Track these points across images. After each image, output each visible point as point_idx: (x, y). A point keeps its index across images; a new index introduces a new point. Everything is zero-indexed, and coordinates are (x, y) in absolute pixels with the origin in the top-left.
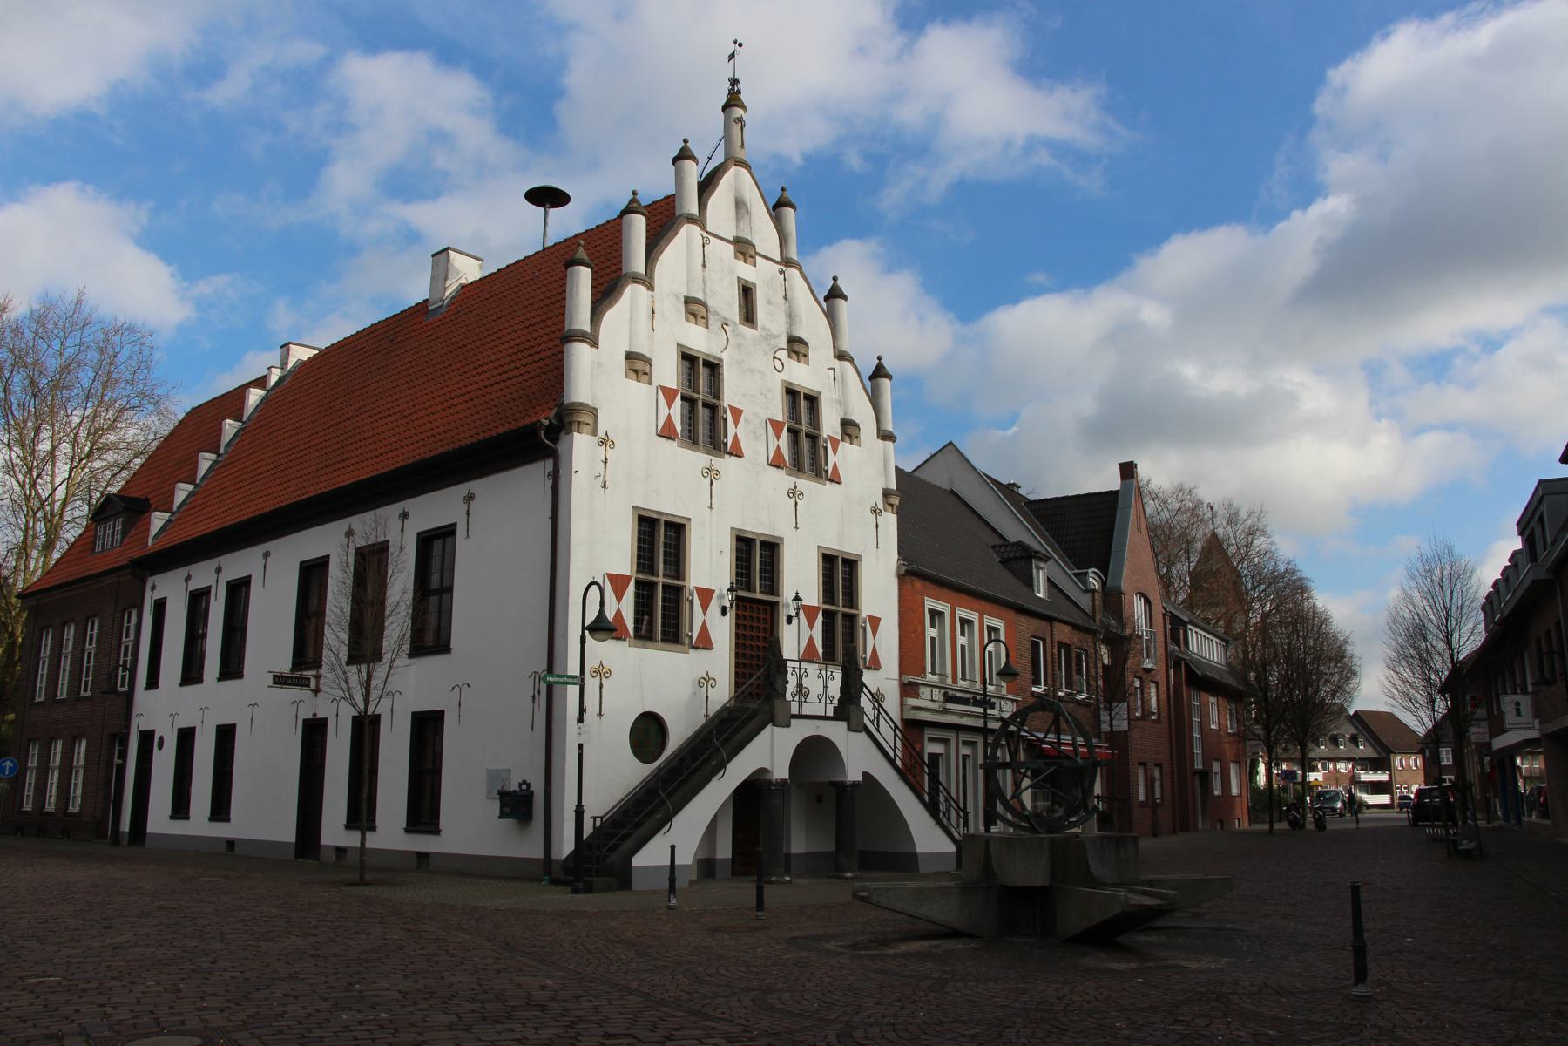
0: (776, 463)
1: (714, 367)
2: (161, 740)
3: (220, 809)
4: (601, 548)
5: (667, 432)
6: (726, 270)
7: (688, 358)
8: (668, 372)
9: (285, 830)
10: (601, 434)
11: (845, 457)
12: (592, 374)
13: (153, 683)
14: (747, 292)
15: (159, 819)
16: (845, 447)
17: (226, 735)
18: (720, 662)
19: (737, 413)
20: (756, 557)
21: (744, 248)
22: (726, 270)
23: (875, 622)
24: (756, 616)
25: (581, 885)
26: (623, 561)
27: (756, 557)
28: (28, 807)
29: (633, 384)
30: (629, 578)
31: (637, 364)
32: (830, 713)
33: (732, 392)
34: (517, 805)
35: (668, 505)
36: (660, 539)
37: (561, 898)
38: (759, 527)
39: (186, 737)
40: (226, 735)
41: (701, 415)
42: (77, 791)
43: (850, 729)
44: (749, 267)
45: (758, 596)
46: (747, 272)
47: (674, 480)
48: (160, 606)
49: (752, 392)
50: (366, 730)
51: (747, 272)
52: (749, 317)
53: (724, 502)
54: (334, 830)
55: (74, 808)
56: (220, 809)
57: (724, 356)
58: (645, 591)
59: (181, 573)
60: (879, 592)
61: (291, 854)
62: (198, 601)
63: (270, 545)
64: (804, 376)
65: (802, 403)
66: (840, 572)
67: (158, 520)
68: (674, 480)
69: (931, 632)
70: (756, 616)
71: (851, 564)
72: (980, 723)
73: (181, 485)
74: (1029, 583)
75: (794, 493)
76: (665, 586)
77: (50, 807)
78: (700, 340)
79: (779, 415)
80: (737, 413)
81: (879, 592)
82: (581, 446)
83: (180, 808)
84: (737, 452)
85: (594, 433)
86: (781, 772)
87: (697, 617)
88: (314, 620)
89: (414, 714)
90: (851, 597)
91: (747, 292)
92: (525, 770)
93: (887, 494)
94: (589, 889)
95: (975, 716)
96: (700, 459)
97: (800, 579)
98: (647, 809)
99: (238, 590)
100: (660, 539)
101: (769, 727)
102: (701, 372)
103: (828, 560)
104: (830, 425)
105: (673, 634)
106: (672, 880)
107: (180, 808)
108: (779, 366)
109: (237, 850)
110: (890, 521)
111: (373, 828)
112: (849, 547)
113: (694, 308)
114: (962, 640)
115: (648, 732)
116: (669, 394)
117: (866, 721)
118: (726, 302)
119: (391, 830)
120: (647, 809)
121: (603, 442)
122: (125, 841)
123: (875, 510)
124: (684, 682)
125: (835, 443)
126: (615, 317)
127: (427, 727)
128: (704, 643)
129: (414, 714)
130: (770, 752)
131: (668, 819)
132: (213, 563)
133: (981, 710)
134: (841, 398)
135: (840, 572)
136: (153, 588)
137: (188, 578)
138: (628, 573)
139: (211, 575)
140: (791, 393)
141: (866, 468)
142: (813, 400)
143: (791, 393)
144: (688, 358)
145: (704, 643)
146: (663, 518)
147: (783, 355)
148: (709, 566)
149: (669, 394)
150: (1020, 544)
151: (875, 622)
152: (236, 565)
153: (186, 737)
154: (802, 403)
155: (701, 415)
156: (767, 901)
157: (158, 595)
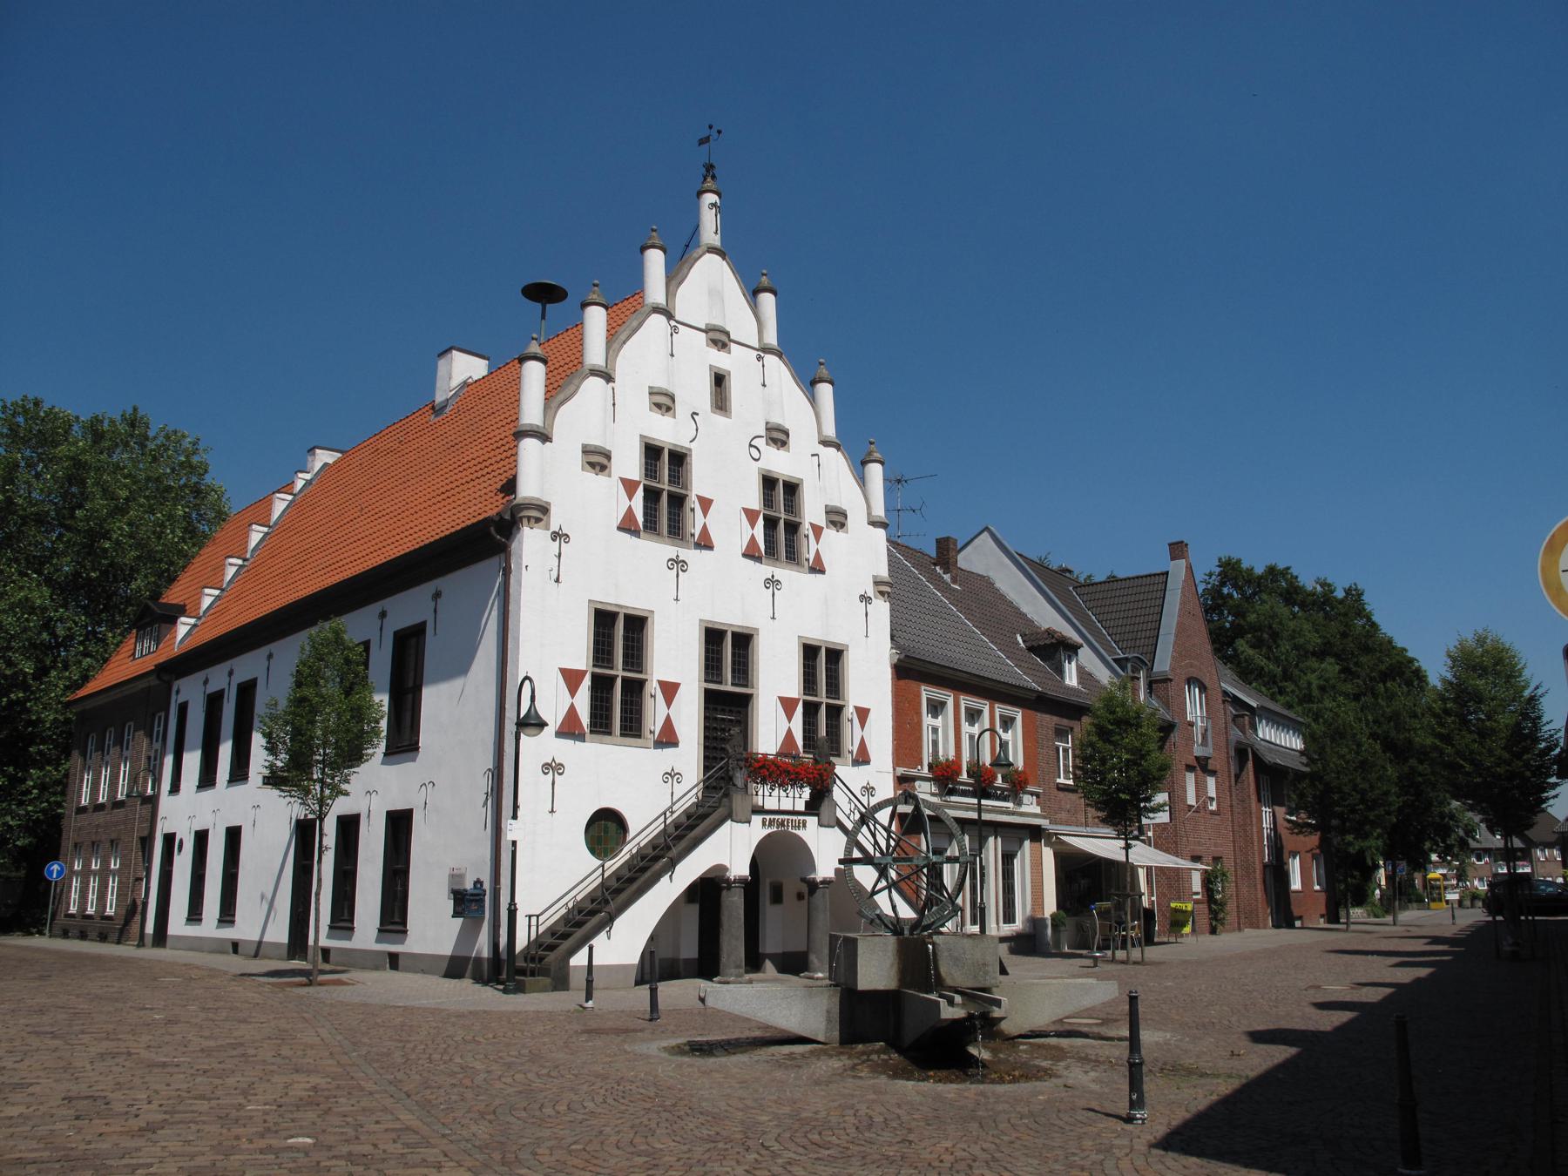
0: (751, 554)
1: (679, 459)
2: (181, 841)
3: (228, 913)
4: (550, 640)
5: (627, 526)
6: (699, 359)
7: (652, 452)
8: (629, 463)
9: (279, 933)
10: (554, 527)
11: (831, 545)
12: (541, 471)
13: (175, 789)
14: (719, 380)
15: (177, 923)
16: (830, 534)
17: (233, 835)
18: (689, 757)
19: (706, 504)
20: (728, 650)
21: (719, 339)
22: (699, 359)
23: (863, 714)
24: (727, 711)
25: (511, 985)
26: (580, 656)
27: (728, 650)
28: (73, 910)
29: (590, 476)
30: (584, 672)
31: (597, 460)
32: (801, 806)
33: (700, 481)
34: (466, 902)
35: (627, 599)
36: (619, 634)
37: (489, 997)
38: (731, 617)
39: (201, 838)
40: (233, 835)
41: (663, 498)
42: (111, 898)
43: (821, 825)
44: (722, 354)
45: (729, 688)
46: (721, 360)
47: (637, 574)
48: (183, 709)
49: (725, 486)
50: (349, 827)
51: (721, 360)
52: (721, 403)
53: (683, 599)
54: (320, 933)
55: (110, 912)
56: (228, 913)
57: (692, 446)
58: (601, 686)
59: (199, 677)
60: (869, 682)
61: (284, 952)
62: (214, 702)
63: (273, 647)
64: (781, 464)
65: (780, 494)
66: (822, 664)
67: (183, 626)
68: (637, 574)
69: (928, 720)
70: (727, 711)
71: (835, 656)
72: (974, 815)
73: (207, 591)
74: (1060, 671)
75: (772, 583)
76: (624, 680)
77: (90, 911)
78: (667, 432)
79: (755, 503)
80: (706, 504)
81: (869, 682)
82: (531, 543)
83: (195, 914)
84: (705, 543)
85: (547, 528)
86: (740, 868)
87: (655, 712)
88: (410, 696)
89: (389, 814)
90: (835, 686)
91: (719, 380)
92: (477, 870)
93: (877, 583)
94: (520, 989)
95: (967, 808)
96: (670, 550)
97: (776, 678)
98: (594, 912)
99: (247, 691)
100: (619, 634)
101: (729, 822)
102: (669, 465)
103: (810, 652)
104: (812, 512)
105: (633, 727)
106: (589, 982)
107: (195, 914)
108: (756, 455)
109: (332, 956)
110: (881, 610)
111: (1239, 561)
112: (835, 637)
113: (663, 402)
114: (966, 728)
115: (605, 828)
116: (629, 486)
117: (839, 814)
118: (695, 392)
119: (209, 926)
120: (594, 912)
121: (556, 536)
122: (149, 940)
123: (865, 598)
124: (649, 782)
125: (817, 531)
126: (566, 415)
127: (399, 825)
128: (668, 738)
129: (389, 814)
130: (731, 849)
131: (610, 920)
132: (224, 667)
133: (975, 801)
134: (827, 480)
135: (822, 664)
136: (178, 692)
137: (206, 682)
138: (584, 668)
139: (219, 678)
140: (769, 482)
141: (859, 554)
142: (792, 488)
143: (769, 482)
144: (652, 452)
145: (668, 738)
146: (623, 611)
147: (760, 443)
148: (674, 658)
149: (629, 486)
150: (1050, 633)
151: (863, 714)
152: (247, 666)
153: (201, 838)
154: (780, 494)
155: (663, 498)
156: (662, 1004)
157: (181, 699)
